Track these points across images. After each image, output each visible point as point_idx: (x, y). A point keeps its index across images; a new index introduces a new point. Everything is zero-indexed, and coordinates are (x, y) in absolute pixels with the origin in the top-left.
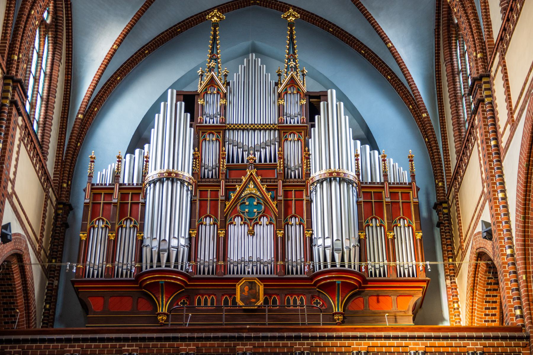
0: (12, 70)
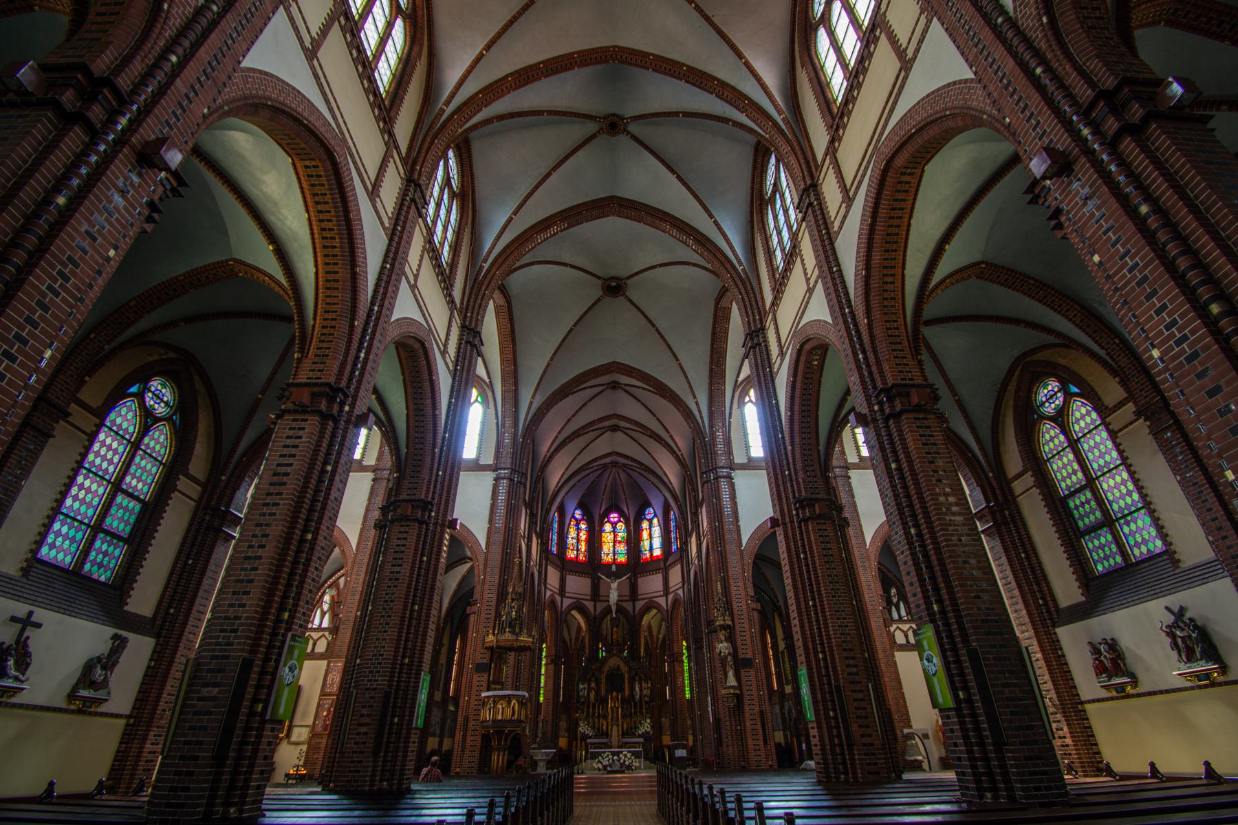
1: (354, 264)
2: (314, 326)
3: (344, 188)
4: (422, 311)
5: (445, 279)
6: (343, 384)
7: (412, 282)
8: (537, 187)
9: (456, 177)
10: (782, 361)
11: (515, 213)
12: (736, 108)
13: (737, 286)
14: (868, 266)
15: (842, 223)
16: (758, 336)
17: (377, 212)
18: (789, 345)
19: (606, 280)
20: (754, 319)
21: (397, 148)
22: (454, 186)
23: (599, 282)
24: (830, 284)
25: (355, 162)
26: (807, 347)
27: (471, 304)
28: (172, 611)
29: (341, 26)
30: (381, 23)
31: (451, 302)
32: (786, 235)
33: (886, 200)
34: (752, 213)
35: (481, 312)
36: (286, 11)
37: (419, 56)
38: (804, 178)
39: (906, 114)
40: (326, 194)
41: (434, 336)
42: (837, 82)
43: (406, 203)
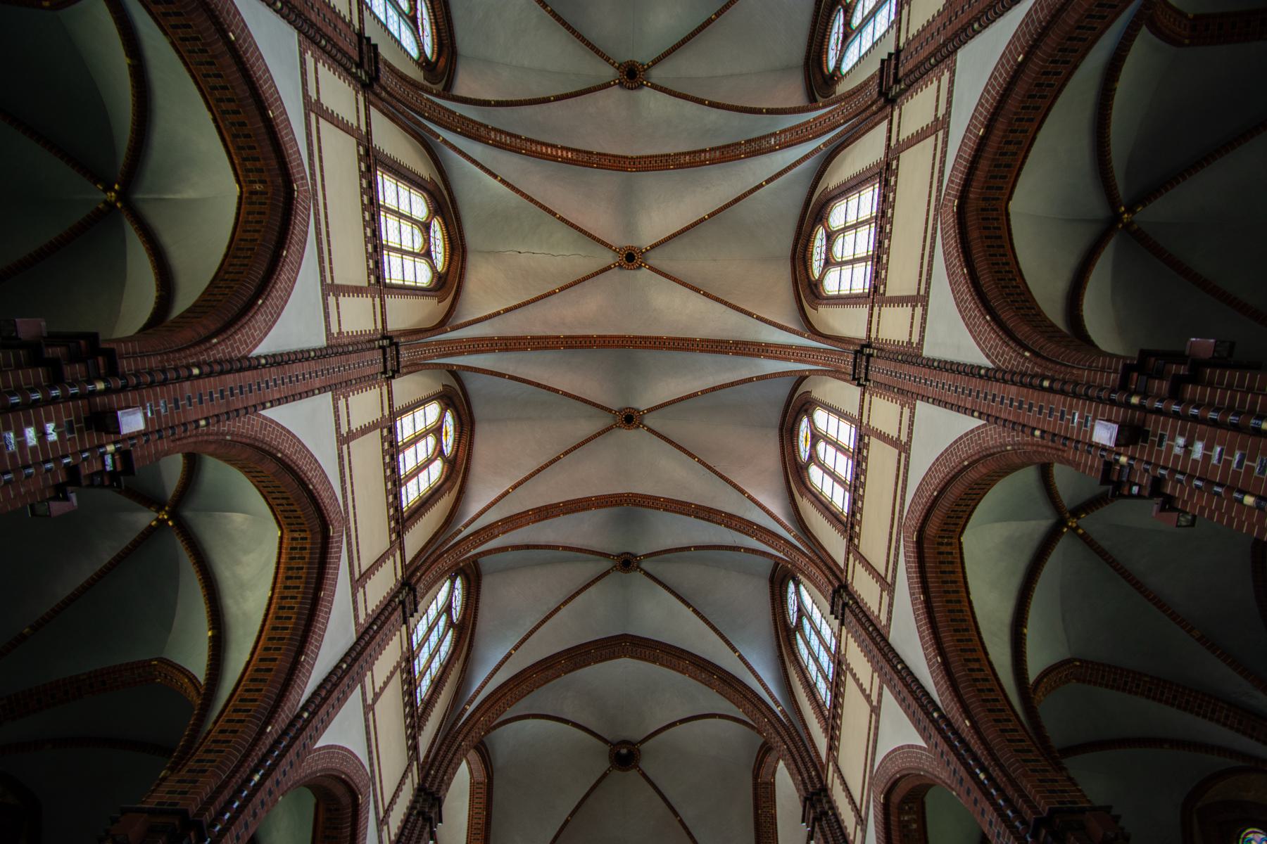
1: (301, 650)
2: (210, 731)
3: (326, 563)
4: (369, 746)
5: (415, 718)
6: (207, 818)
7: (369, 701)
8: (543, 622)
9: (458, 609)
10: (864, 831)
11: (516, 648)
12: (747, 534)
13: (779, 733)
14: (940, 648)
15: (890, 612)
16: (820, 801)
17: (355, 602)
18: (868, 802)
19: (614, 745)
20: (810, 777)
21: (418, 759)
22: (454, 618)
23: (607, 748)
24: (900, 686)
25: (349, 544)
26: (896, 798)
27: (439, 758)
29: (382, 435)
30: (422, 457)
31: (414, 748)
32: (824, 659)
33: (932, 572)
34: (781, 655)
35: (450, 770)
36: (333, 400)
37: (450, 489)
38: (830, 582)
39: (921, 484)
40: (302, 568)
41: (375, 790)
42: (839, 499)
43: (393, 604)
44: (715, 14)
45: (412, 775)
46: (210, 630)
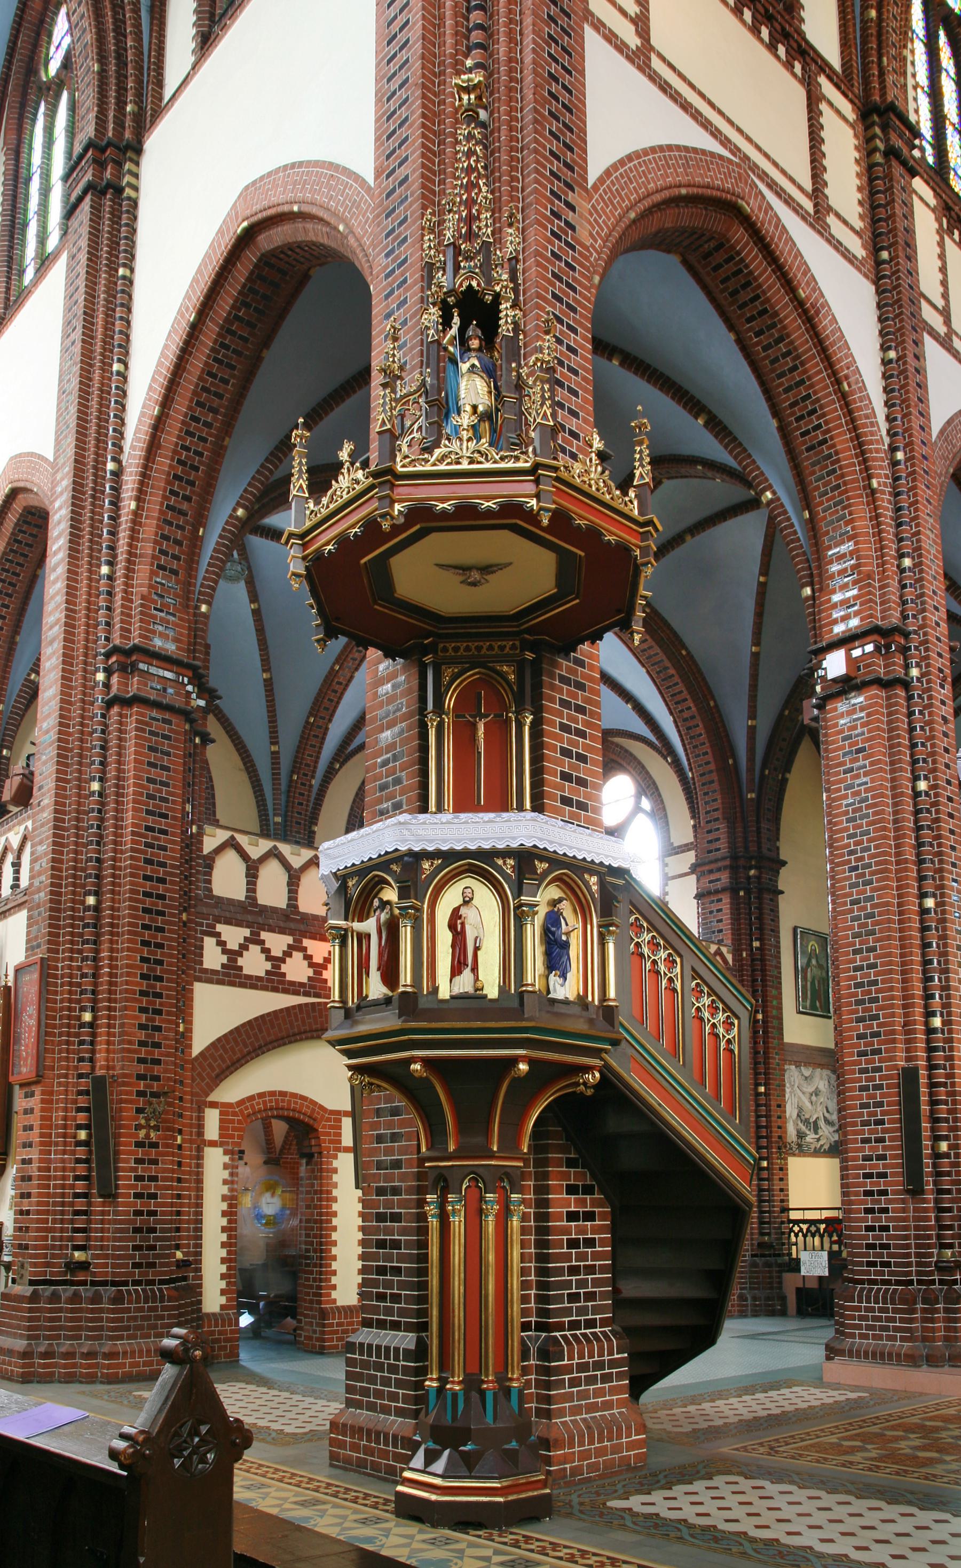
0: (873, 95)
7: (633, 41)
21: (824, 67)
28: (91, 900)
44: (264, 671)
45: (831, 104)
46: (610, 360)
